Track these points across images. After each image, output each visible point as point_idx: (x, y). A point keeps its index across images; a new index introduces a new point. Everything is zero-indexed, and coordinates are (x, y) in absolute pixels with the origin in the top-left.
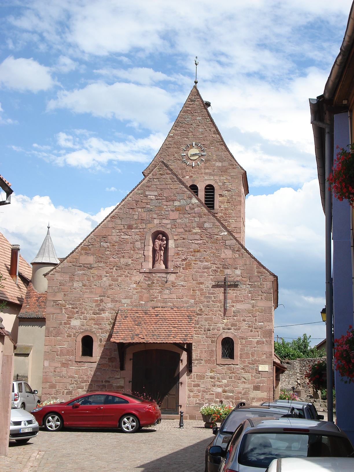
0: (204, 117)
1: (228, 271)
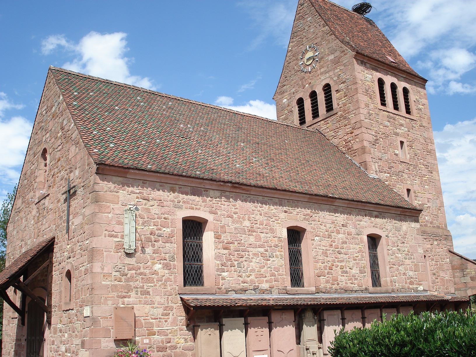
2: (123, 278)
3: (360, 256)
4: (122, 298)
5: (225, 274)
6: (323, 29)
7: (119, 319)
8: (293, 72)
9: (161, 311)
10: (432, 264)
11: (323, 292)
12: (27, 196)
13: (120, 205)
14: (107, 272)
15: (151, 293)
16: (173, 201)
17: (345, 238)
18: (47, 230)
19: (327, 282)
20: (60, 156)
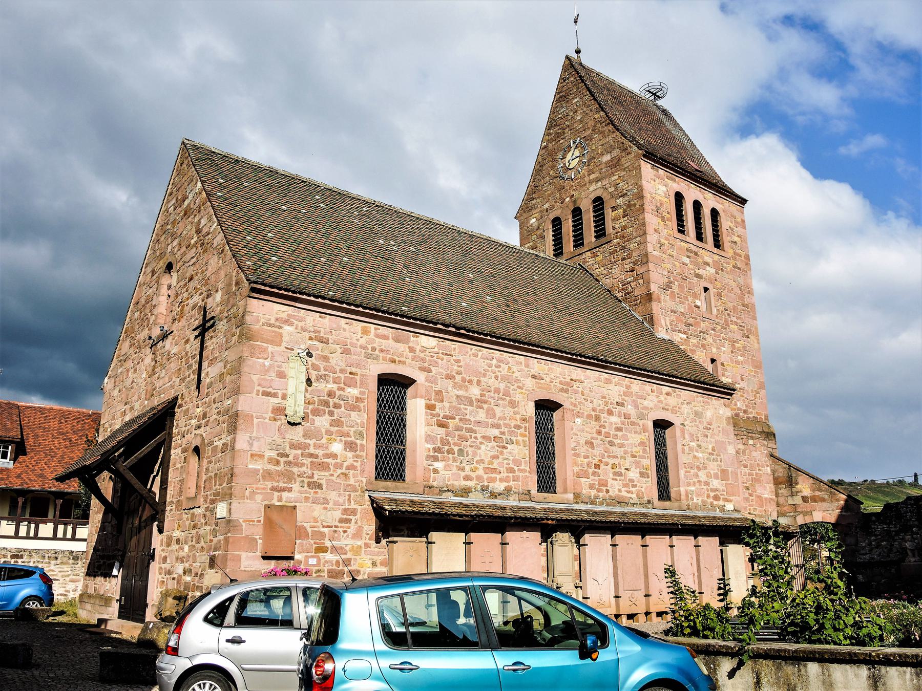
0: (582, 96)
2: (282, 460)
3: (641, 451)
4: (279, 491)
5: (438, 465)
6: (596, 116)
7: (269, 524)
8: (547, 179)
9: (338, 514)
10: (745, 472)
11: (585, 503)
12: (138, 336)
13: (282, 348)
14: (257, 450)
15: (324, 487)
16: (365, 348)
17: (620, 423)
18: (166, 385)
19: (591, 487)
20: (193, 273)
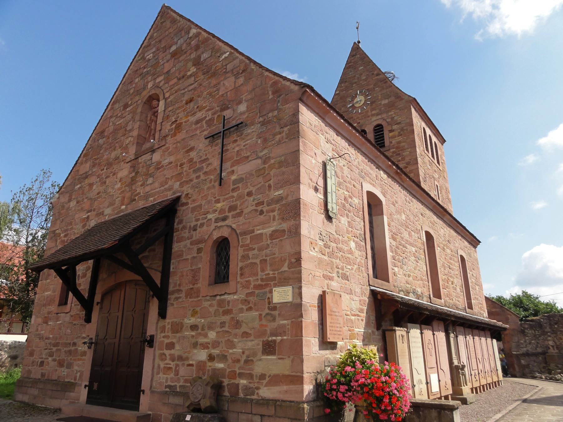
1: (228, 113)
